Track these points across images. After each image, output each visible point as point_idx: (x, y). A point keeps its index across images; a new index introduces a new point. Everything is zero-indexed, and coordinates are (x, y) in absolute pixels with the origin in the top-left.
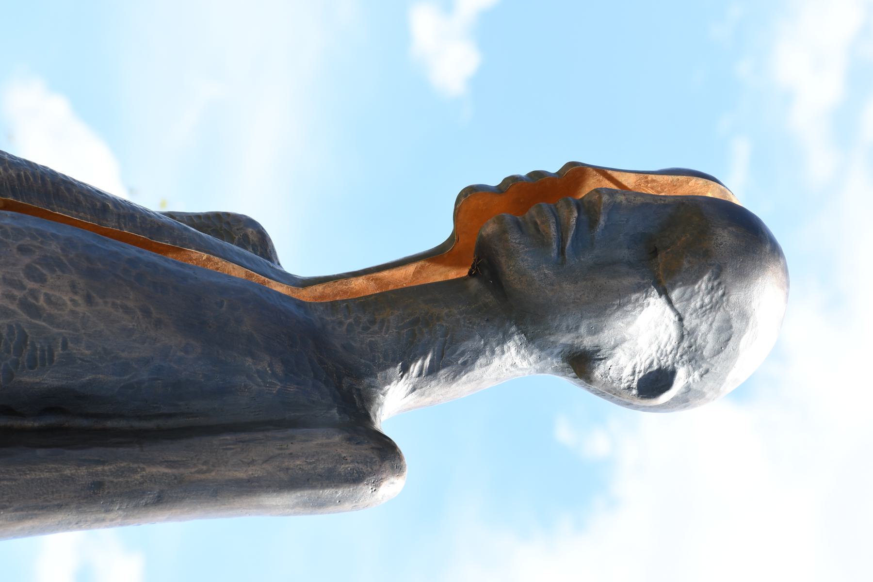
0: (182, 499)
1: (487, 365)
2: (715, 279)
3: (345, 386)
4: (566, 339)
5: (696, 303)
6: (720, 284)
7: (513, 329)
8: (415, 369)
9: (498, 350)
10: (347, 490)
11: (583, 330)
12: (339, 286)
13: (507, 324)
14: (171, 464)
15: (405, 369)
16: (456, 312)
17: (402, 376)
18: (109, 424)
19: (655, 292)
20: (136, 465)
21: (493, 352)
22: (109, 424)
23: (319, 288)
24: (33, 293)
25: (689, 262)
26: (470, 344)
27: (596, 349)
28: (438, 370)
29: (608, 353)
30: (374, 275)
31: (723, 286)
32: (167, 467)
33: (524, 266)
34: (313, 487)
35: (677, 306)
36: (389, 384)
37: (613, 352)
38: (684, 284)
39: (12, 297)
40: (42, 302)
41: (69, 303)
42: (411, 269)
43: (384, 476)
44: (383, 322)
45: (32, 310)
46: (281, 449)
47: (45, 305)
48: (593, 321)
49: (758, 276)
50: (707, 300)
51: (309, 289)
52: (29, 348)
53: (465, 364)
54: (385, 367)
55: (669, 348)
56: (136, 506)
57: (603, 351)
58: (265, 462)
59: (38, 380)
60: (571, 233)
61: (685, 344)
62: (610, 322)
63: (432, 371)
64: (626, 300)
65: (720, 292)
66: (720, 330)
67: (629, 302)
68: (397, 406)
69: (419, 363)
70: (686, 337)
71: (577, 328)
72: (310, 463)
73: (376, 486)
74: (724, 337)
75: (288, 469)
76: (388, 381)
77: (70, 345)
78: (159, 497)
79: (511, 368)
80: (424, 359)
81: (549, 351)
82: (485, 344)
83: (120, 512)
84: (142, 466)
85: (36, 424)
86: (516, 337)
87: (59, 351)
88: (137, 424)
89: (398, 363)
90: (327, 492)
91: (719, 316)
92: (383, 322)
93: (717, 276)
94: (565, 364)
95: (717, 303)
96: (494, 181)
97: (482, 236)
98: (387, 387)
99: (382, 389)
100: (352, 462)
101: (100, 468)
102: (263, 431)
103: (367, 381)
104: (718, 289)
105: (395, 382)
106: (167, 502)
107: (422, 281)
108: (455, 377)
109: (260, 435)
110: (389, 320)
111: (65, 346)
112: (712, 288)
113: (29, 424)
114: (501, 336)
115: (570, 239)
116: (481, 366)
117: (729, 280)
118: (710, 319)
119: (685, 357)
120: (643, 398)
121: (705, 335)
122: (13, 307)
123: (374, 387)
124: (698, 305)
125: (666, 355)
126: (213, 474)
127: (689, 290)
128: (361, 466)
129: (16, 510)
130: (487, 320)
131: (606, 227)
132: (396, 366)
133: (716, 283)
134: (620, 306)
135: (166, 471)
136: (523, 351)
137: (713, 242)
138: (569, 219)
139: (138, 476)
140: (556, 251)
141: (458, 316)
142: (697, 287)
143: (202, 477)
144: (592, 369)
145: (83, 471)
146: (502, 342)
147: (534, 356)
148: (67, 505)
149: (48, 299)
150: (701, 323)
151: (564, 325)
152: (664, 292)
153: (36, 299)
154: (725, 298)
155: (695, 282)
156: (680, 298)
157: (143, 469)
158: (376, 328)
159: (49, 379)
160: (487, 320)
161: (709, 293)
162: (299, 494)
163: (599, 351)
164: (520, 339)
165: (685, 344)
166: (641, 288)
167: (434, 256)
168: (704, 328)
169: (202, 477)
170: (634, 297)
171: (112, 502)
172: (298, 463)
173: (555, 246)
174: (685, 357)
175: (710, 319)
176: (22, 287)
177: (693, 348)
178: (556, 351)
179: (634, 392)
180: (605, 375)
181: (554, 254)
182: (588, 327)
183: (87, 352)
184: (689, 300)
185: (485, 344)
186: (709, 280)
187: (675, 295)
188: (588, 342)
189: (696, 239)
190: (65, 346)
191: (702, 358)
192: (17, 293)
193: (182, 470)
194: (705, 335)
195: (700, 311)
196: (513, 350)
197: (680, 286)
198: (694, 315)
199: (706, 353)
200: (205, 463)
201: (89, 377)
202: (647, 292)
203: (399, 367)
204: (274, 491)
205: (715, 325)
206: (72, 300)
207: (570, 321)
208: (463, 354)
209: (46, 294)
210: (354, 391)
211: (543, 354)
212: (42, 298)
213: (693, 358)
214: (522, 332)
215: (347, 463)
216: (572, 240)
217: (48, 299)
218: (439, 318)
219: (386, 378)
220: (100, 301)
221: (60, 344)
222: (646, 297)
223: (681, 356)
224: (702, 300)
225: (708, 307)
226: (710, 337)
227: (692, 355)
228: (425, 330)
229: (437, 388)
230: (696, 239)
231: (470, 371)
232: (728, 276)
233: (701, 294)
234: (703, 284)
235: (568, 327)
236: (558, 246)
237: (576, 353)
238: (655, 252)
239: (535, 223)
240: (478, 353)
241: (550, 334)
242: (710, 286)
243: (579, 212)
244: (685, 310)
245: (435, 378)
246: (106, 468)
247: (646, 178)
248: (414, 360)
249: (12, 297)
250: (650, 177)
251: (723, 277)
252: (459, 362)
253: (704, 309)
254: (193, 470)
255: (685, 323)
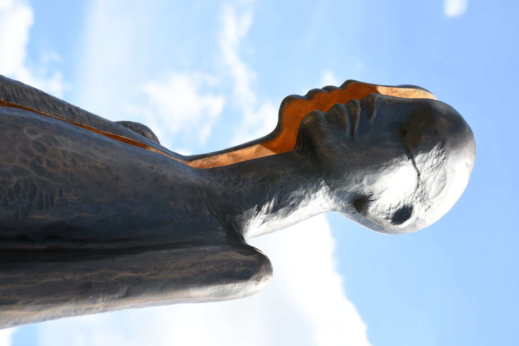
0: (143, 292)
1: (306, 206)
2: (441, 149)
3: (228, 220)
4: (353, 188)
5: (429, 164)
6: (443, 152)
7: (323, 182)
8: (265, 209)
9: (313, 195)
10: (241, 284)
11: (365, 182)
12: (212, 160)
13: (319, 180)
14: (134, 270)
15: (259, 209)
16: (288, 172)
17: (257, 214)
18: (89, 246)
19: (406, 157)
20: (111, 272)
21: (310, 197)
22: (89, 246)
23: (200, 162)
24: (39, 159)
25: (426, 138)
26: (297, 193)
27: (371, 194)
28: (278, 209)
29: (377, 196)
30: (232, 153)
31: (445, 153)
32: (131, 272)
33: (329, 141)
34: (221, 283)
35: (418, 166)
36: (250, 219)
37: (380, 195)
38: (423, 152)
39: (26, 162)
40: (44, 165)
41: (62, 165)
42: (254, 148)
43: (262, 274)
44: (244, 179)
45: (40, 171)
46: (200, 259)
47: (46, 167)
48: (371, 176)
49: (463, 147)
50: (435, 161)
51: (194, 162)
52: (38, 195)
53: (293, 205)
54: (247, 208)
55: (410, 193)
56: (113, 299)
57: (374, 195)
58: (191, 267)
59: (44, 217)
60: (358, 121)
61: (419, 190)
62: (381, 177)
63: (275, 210)
64: (390, 162)
65: (443, 157)
66: (440, 181)
67: (392, 164)
68: (259, 231)
69: (267, 205)
70: (420, 185)
71: (362, 180)
72: (219, 267)
73: (258, 281)
74: (442, 185)
75: (205, 271)
76: (249, 217)
77: (64, 193)
78: (127, 292)
79: (318, 209)
80: (270, 203)
81: (342, 196)
82: (305, 193)
83: (103, 303)
84: (115, 272)
85: (42, 247)
86: (324, 188)
87: (57, 198)
88: (107, 246)
89: (255, 205)
90: (229, 286)
91: (441, 172)
92: (244, 179)
93: (442, 147)
94: (350, 205)
95: (441, 163)
96: (303, 92)
97: (304, 124)
98: (249, 221)
99: (246, 222)
100: (243, 266)
101: (88, 274)
102: (186, 247)
103: (238, 217)
104: (441, 155)
105: (254, 217)
106: (132, 295)
107: (260, 156)
108: (287, 214)
109: (184, 250)
110: (248, 179)
111: (61, 194)
112: (439, 155)
113: (38, 247)
114: (315, 187)
115: (357, 125)
116: (303, 206)
117: (448, 150)
118: (436, 174)
119: (418, 199)
120: (395, 224)
121: (431, 184)
122: (27, 167)
123: (242, 220)
124: (430, 165)
125: (408, 197)
126: (160, 276)
127: (426, 156)
128: (248, 268)
129: (36, 304)
130: (307, 177)
131: (377, 117)
132: (254, 208)
133: (441, 151)
134: (387, 166)
135: (131, 275)
136: (326, 197)
137: (439, 126)
138: (356, 112)
139: (113, 279)
140: (349, 133)
141: (290, 175)
142: (430, 153)
143: (154, 277)
144: (367, 207)
145: (78, 277)
146: (316, 190)
147: (333, 199)
148: (69, 299)
149: (48, 162)
150: (430, 176)
151: (354, 179)
152: (411, 157)
153: (41, 163)
154: (445, 160)
155: (429, 151)
156: (420, 161)
157: (116, 274)
158: (241, 183)
159: (49, 217)
160: (307, 177)
161: (437, 157)
162: (212, 288)
163: (372, 195)
164: (326, 189)
165: (419, 190)
166: (399, 155)
167: (264, 142)
168: (431, 180)
169: (154, 277)
170: (395, 160)
171: (98, 296)
172: (211, 267)
173: (348, 129)
174: (418, 199)
175: (436, 174)
176: (32, 155)
177: (423, 192)
178: (346, 196)
179: (390, 221)
180: (375, 209)
181: (348, 135)
182: (368, 180)
183: (75, 198)
184: (424, 162)
185: (305, 193)
186: (437, 149)
187: (417, 159)
188: (366, 190)
189: (422, 127)
190: (61, 194)
191: (428, 199)
192: (30, 159)
193: (140, 274)
194: (431, 184)
195: (430, 169)
196: (321, 196)
197: (421, 153)
198: (427, 172)
199: (430, 196)
200: (155, 269)
201: (76, 215)
202: (402, 157)
203: (255, 208)
204: (198, 286)
205: (437, 178)
206: (64, 164)
207: (358, 176)
208: (292, 199)
209: (47, 160)
210: (233, 223)
211: (338, 198)
212: (44, 162)
213: (423, 199)
214: (328, 184)
215: (240, 267)
216: (358, 127)
217: (48, 162)
218: (278, 177)
219: (248, 215)
220: (81, 164)
221: (58, 193)
222: (401, 161)
223: (416, 198)
224: (432, 162)
225: (435, 166)
226: (434, 186)
227: (422, 197)
228: (270, 184)
229: (277, 220)
230: (422, 127)
231: (296, 209)
232: (447, 146)
233: (432, 157)
234: (434, 151)
235: (356, 180)
236: (350, 129)
237: (358, 197)
238: (404, 133)
239: (336, 116)
240: (301, 198)
241: (345, 185)
242: (438, 152)
243: (362, 108)
244: (422, 168)
245: (276, 214)
246: (93, 274)
247: (392, 90)
248: (264, 203)
249: (26, 162)
250: (394, 89)
251: (445, 148)
252: (290, 204)
253: (433, 167)
254: (148, 274)
255: (421, 176)
